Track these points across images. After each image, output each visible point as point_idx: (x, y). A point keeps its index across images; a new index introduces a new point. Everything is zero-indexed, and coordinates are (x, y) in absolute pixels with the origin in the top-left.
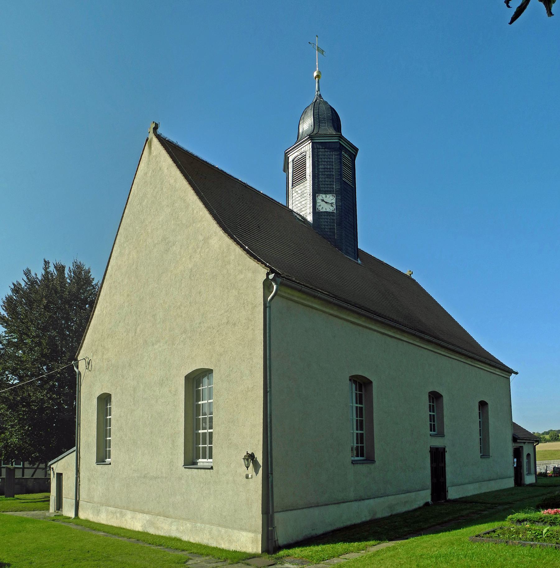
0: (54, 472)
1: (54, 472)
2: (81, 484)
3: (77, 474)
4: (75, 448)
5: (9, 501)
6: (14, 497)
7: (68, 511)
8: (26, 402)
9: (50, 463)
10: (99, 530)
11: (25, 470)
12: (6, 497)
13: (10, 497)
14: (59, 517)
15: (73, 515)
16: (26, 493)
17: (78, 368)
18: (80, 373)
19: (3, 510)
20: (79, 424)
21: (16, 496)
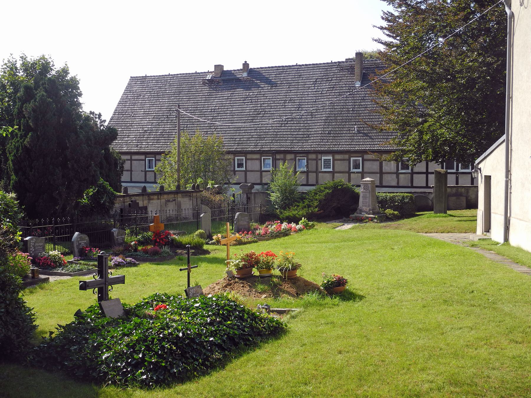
0: (481, 175)
1: (481, 175)
2: (512, 191)
3: (507, 177)
4: (504, 137)
5: (438, 219)
6: (446, 213)
7: (497, 234)
8: (449, 74)
9: (477, 162)
10: (517, 262)
11: (415, 176)
12: (436, 213)
13: (440, 212)
14: (486, 243)
15: (501, 240)
16: (466, 208)
17: (510, 7)
18: (512, 15)
19: (427, 230)
20: (510, 98)
21: (449, 212)
